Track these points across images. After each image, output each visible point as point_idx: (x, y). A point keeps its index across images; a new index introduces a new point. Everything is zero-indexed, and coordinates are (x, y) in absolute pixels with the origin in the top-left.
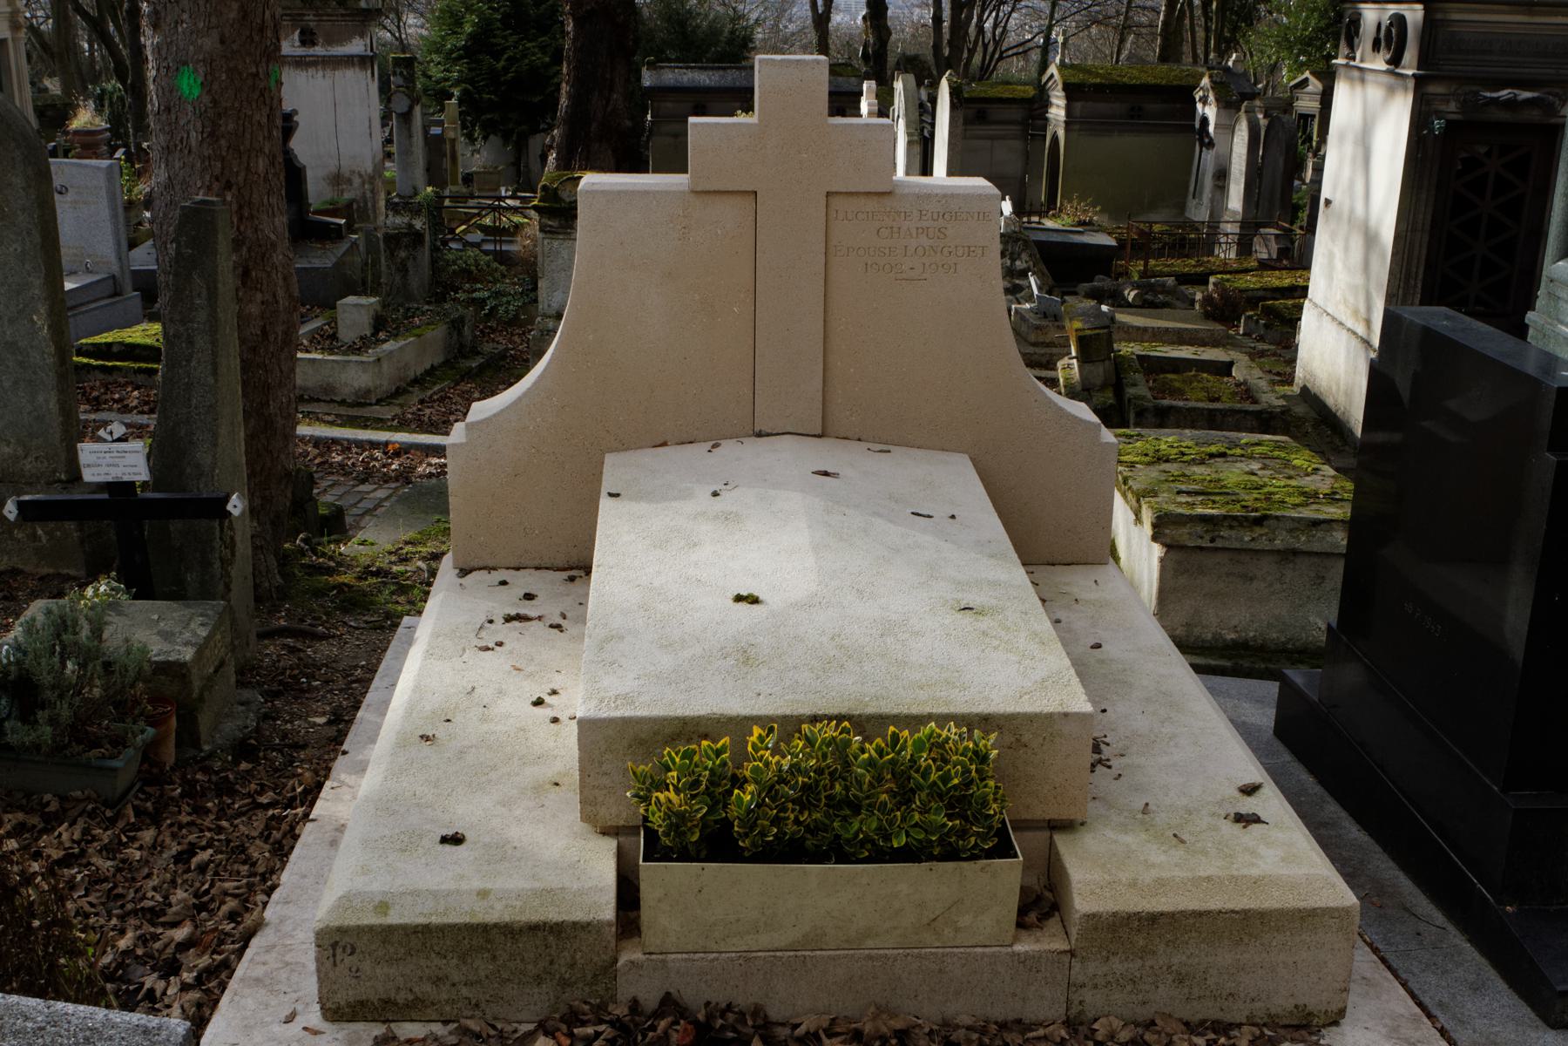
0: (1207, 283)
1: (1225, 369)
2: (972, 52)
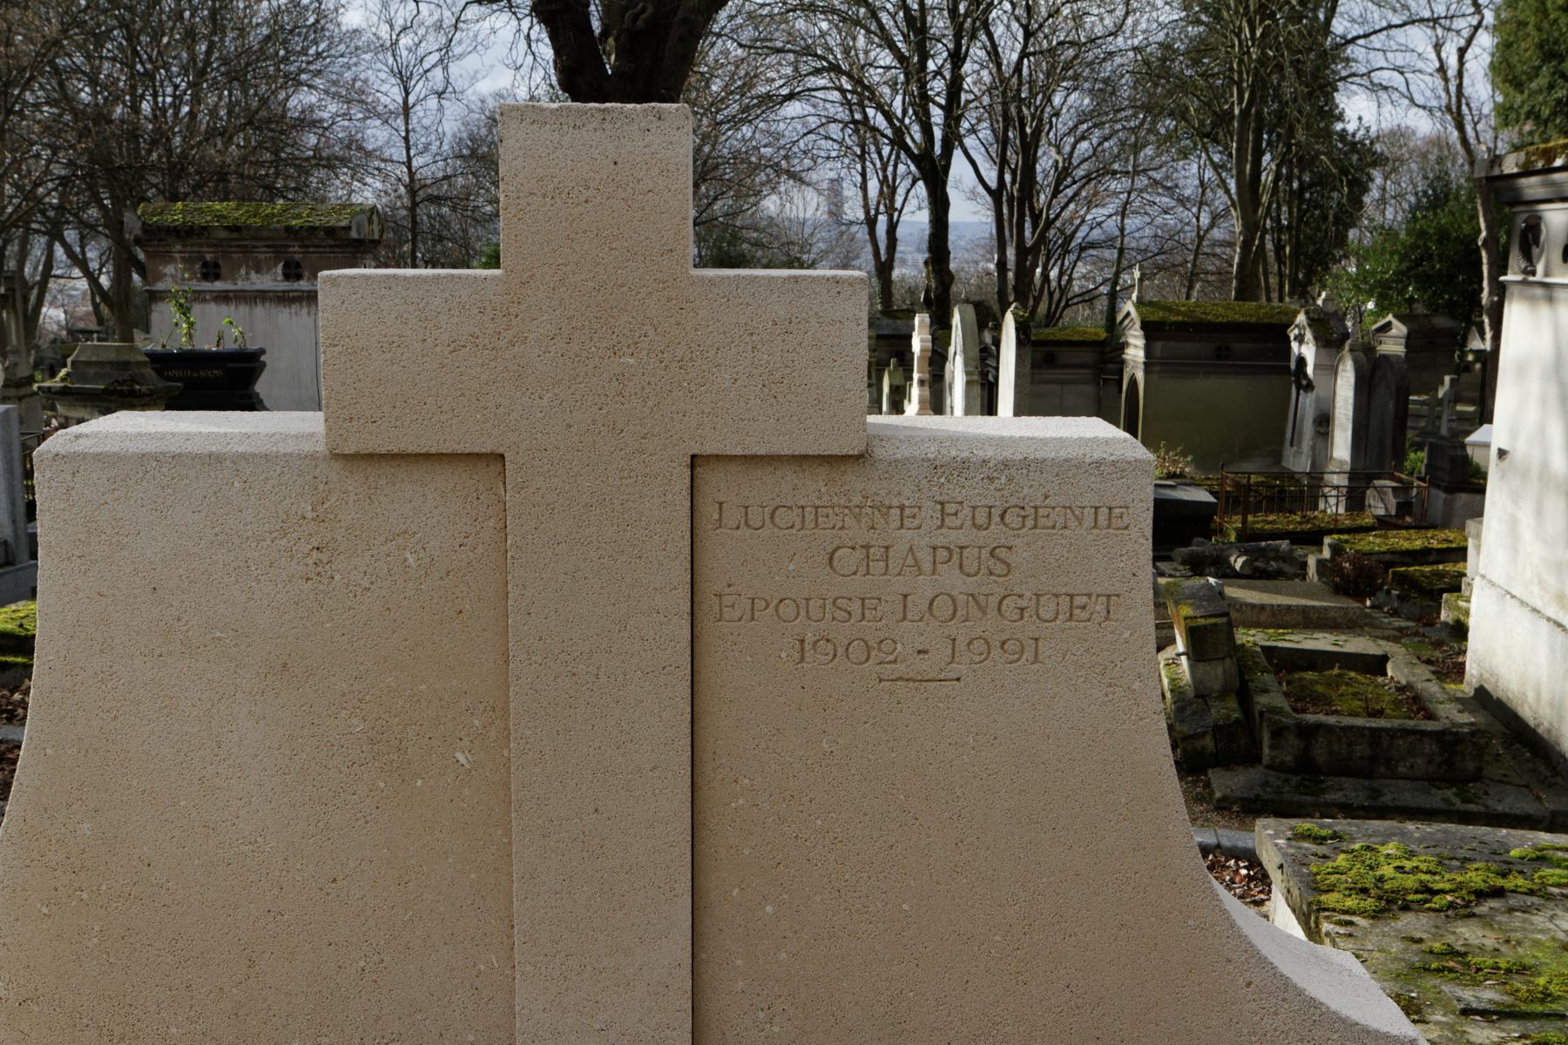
0: (1321, 543)
1: (1376, 665)
2: (1037, 300)
